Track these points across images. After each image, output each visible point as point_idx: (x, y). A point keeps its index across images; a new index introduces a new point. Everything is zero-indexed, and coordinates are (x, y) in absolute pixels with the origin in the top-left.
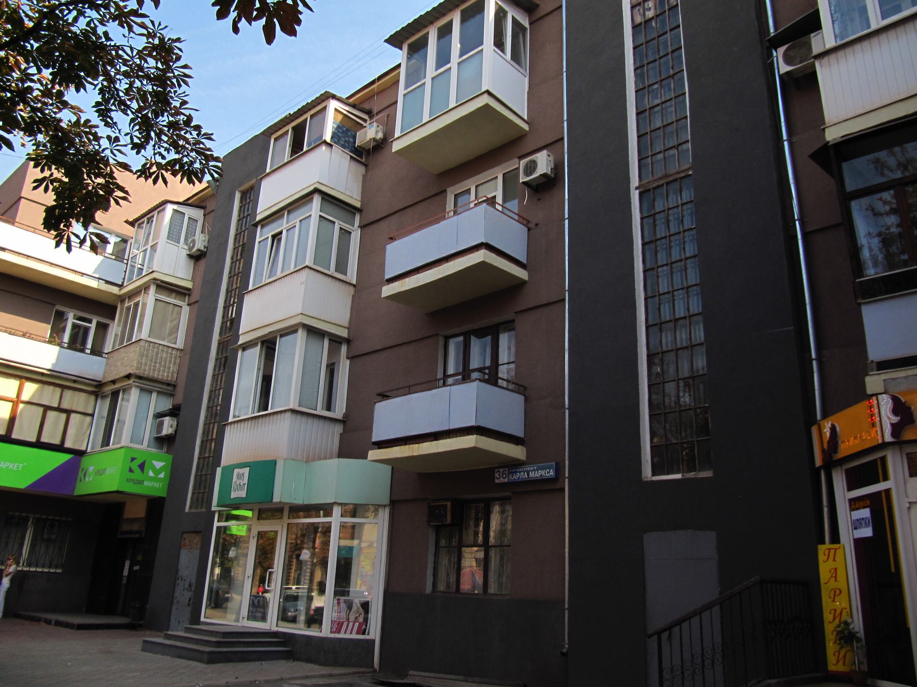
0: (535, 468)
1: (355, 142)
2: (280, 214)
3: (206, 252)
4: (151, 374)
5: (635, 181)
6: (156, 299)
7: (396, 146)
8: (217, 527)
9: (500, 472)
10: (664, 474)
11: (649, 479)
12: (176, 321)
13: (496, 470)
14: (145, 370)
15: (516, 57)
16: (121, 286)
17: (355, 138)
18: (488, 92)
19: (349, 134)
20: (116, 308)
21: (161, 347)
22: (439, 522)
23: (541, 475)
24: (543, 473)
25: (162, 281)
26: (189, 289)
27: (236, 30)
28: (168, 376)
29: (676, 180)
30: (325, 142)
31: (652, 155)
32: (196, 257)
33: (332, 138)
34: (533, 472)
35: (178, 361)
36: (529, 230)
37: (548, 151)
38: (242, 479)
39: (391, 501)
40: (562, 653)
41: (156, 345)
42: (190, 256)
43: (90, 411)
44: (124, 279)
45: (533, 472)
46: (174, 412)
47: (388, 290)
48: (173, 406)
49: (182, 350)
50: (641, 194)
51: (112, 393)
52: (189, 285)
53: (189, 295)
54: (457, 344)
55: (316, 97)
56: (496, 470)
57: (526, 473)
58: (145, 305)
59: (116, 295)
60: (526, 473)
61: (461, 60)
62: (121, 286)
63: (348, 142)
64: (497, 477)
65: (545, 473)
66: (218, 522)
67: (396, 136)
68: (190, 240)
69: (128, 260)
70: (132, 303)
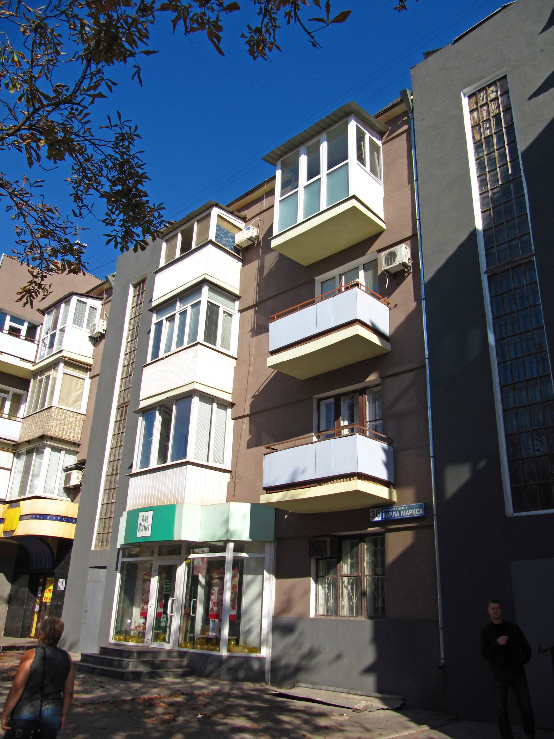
0: (406, 507)
1: (234, 242)
2: (172, 301)
3: (105, 334)
4: (60, 435)
5: (484, 267)
6: (64, 373)
7: (275, 243)
8: (122, 562)
9: (374, 511)
10: (525, 511)
11: (511, 515)
12: (80, 391)
13: (370, 510)
14: (56, 432)
15: (373, 170)
16: (34, 363)
17: (233, 238)
18: (354, 197)
19: (229, 235)
20: (29, 382)
21: (68, 413)
22: (320, 556)
23: (412, 514)
24: (414, 512)
25: (69, 359)
26: (90, 365)
27: (71, 195)
28: (74, 436)
29: (520, 265)
30: (211, 242)
31: (497, 246)
32: (96, 340)
33: (216, 238)
34: (405, 511)
35: (82, 424)
36: (390, 309)
37: (406, 244)
38: (147, 520)
39: (275, 537)
40: (439, 667)
41: (61, 410)
42: (92, 338)
43: (9, 467)
44: (36, 357)
45: (405, 511)
46: (80, 466)
47: (273, 360)
48: (78, 461)
49: (85, 415)
50: (489, 277)
51: (27, 451)
52: (91, 361)
53: (91, 370)
54: (328, 405)
55: (392, 104)
56: (370, 510)
57: (398, 512)
58: (55, 379)
59: (29, 370)
60: (398, 512)
61: (329, 171)
62: (34, 363)
63: (229, 241)
64: (371, 516)
65: (415, 512)
66: (122, 557)
67: (274, 235)
68: (91, 325)
69: (39, 342)
70: (44, 377)
